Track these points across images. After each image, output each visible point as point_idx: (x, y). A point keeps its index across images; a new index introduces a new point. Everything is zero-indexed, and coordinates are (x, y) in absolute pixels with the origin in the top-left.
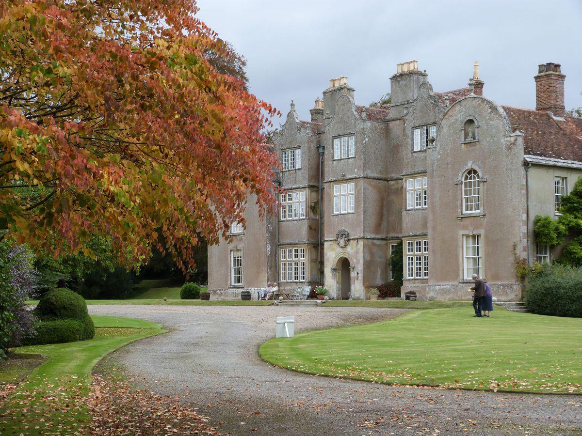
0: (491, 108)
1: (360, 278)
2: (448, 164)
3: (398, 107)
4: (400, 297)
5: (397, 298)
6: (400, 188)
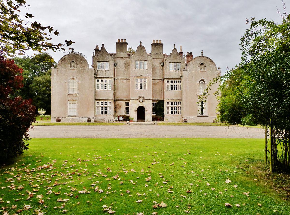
0: (210, 61)
1: (150, 114)
2: (193, 77)
3: (155, 55)
4: (164, 121)
5: (162, 121)
6: (156, 83)
